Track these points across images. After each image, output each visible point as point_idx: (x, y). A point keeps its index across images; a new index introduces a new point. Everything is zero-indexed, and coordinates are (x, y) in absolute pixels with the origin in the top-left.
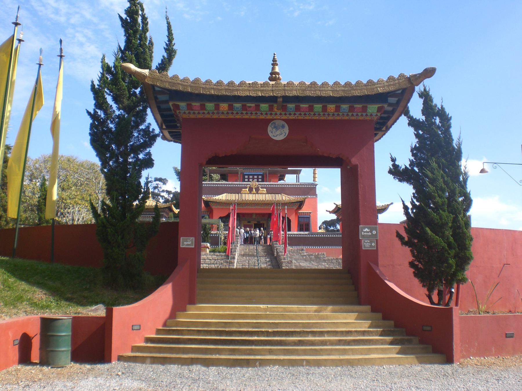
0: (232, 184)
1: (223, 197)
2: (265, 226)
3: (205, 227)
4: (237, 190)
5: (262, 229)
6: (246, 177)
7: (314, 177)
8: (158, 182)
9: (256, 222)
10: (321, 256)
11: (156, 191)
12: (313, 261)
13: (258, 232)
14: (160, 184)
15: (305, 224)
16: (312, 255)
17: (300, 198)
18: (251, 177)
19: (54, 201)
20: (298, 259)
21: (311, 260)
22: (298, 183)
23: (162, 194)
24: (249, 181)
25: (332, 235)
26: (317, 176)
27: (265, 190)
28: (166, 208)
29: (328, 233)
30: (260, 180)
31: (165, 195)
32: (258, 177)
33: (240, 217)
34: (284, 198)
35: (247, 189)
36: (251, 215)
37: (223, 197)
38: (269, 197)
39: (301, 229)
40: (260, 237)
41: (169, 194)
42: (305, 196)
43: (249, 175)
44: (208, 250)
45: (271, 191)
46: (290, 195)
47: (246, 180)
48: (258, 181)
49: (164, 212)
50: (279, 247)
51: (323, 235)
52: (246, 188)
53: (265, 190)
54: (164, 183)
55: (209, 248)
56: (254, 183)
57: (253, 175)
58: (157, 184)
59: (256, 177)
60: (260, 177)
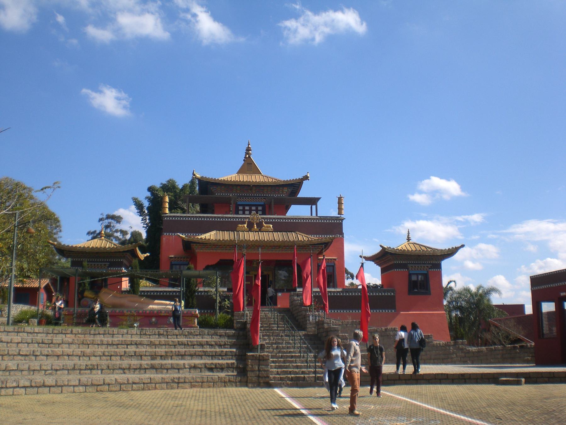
0: (223, 217)
1: (211, 236)
4: (231, 227)
6: (241, 208)
7: (340, 209)
8: (110, 220)
14: (113, 223)
19: (529, 316)
23: (116, 234)
24: (244, 214)
27: (271, 226)
28: (127, 251)
32: (257, 208)
34: (300, 238)
35: (246, 225)
37: (211, 236)
38: (278, 236)
43: (244, 206)
45: (279, 227)
47: (241, 212)
52: (244, 223)
53: (271, 226)
58: (110, 223)
60: (260, 208)
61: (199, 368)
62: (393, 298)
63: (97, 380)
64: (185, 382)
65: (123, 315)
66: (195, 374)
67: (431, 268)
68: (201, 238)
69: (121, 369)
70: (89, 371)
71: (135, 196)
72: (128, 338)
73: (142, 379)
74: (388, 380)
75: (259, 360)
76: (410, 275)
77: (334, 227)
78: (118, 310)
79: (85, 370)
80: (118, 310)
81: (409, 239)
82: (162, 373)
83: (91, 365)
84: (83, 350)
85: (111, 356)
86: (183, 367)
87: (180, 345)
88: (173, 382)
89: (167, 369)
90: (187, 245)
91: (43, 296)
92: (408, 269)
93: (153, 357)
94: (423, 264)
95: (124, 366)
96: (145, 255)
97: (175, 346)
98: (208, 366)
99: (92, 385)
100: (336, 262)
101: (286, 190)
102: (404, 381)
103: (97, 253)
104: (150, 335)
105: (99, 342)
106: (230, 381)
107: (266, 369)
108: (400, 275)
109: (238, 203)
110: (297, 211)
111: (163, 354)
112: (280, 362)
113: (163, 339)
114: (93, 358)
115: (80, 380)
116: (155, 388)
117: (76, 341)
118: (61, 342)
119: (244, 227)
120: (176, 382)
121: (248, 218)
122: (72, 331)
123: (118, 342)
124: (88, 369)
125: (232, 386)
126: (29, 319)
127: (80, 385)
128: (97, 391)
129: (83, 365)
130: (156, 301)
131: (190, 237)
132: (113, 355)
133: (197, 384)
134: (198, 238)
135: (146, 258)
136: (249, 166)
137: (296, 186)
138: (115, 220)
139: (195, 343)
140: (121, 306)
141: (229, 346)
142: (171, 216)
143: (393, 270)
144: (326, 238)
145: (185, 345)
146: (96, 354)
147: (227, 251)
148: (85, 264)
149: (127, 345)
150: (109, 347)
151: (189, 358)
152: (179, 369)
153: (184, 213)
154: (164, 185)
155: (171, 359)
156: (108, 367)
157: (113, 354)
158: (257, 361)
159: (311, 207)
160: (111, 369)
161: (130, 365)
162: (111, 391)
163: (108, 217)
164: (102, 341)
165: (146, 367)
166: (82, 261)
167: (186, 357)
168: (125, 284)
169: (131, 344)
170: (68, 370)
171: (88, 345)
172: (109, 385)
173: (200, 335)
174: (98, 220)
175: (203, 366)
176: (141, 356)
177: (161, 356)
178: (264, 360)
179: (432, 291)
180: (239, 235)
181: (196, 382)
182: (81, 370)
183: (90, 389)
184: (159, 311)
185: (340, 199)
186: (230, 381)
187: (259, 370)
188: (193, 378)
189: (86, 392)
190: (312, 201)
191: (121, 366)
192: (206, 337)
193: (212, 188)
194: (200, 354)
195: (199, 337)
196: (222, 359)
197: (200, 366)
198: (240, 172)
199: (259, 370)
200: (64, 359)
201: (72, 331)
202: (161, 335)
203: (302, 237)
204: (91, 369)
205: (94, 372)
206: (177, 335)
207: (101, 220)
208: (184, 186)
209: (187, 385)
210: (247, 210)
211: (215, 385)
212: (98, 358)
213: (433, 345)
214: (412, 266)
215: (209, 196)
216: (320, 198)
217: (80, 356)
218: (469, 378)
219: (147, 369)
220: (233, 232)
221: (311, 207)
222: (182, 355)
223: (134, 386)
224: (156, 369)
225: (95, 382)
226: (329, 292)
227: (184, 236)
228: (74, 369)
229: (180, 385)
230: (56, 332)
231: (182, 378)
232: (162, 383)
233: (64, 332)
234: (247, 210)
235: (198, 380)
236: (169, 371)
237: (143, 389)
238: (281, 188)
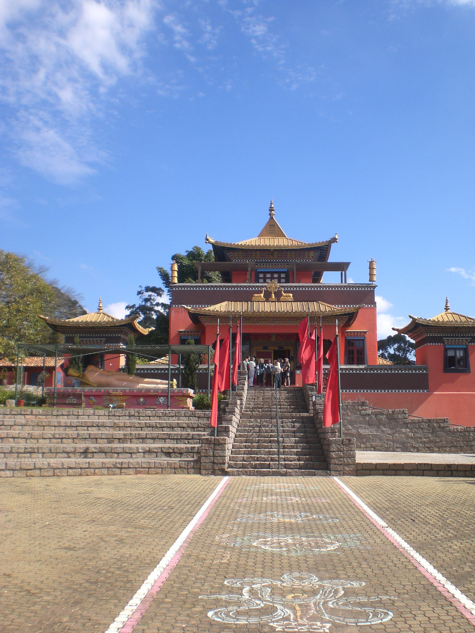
0: (237, 286)
1: (221, 307)
2: (292, 354)
3: (189, 359)
4: (246, 297)
5: (287, 360)
6: (261, 276)
7: (371, 275)
8: (150, 293)
9: (276, 348)
10: (400, 416)
11: (148, 304)
12: (384, 425)
13: (279, 366)
15: (356, 352)
16: (382, 414)
17: (349, 308)
18: (268, 276)
20: (356, 422)
21: (379, 424)
22: (344, 284)
23: (156, 308)
24: (265, 282)
25: (405, 370)
26: (375, 272)
27: (291, 295)
29: (397, 366)
30: (283, 280)
31: (159, 308)
32: (265, 276)
33: (246, 338)
34: (322, 308)
35: (262, 295)
36: (268, 336)
37: (221, 307)
38: (297, 307)
39: (350, 361)
40: (284, 375)
41: (165, 309)
42: (356, 304)
43: (265, 273)
44: (190, 402)
46: (332, 304)
47: (261, 280)
48: (279, 282)
49: (121, 332)
50: (320, 400)
51: (391, 369)
52: (261, 292)
53: (291, 295)
54: (160, 295)
55: (191, 397)
56: (274, 285)
57: (272, 273)
58: (150, 296)
59: (276, 276)
60: (283, 275)
61: (155, 452)
62: (426, 375)
63: (26, 464)
64: (129, 468)
65: (109, 395)
66: (152, 460)
67: (471, 342)
68: (209, 310)
69: (65, 452)
70: (29, 455)
71: (160, 266)
72: (95, 420)
73: (79, 464)
74: (363, 469)
75: (215, 444)
76: (446, 350)
77: (363, 296)
78: (103, 389)
79: (24, 453)
80: (103, 389)
81: (447, 309)
82: (112, 457)
83: (31, 448)
84: (30, 432)
85: (62, 438)
86: (136, 451)
87: (148, 427)
88: (116, 467)
89: (118, 453)
90: (195, 317)
91: (59, 375)
92: (443, 343)
93: (110, 440)
94: (462, 337)
95: (68, 450)
96: (150, 330)
97: (141, 428)
98: (165, 451)
99: (21, 469)
100: (366, 335)
101: (312, 254)
102: (381, 472)
103: (92, 328)
104: (119, 416)
105: (56, 424)
106: (180, 467)
107: (222, 454)
108: (434, 351)
109: (258, 270)
110: (330, 279)
111: (122, 437)
112: (253, 447)
113: (135, 421)
114: (41, 441)
115: (6, 464)
116: (95, 474)
117: (30, 423)
118: (13, 423)
119: (260, 297)
120: (118, 468)
121: (265, 286)
122: (32, 412)
123: (77, 424)
124: (28, 453)
125: (183, 473)
126: (6, 399)
127: (6, 469)
128: (27, 476)
129: (22, 448)
130: (146, 380)
131: (196, 309)
132: (65, 438)
133: (142, 470)
134: (205, 310)
135: (150, 333)
136: (272, 228)
137: (322, 250)
138: (155, 293)
139: (165, 425)
140: (108, 385)
141: (202, 429)
142: (180, 286)
143: (426, 344)
144: (346, 309)
145: (153, 427)
146: (45, 437)
147: (270, 324)
148: (77, 339)
149: (88, 427)
150: (67, 429)
151: (151, 441)
152: (131, 453)
153: (210, 282)
154: (191, 252)
155: (131, 443)
156: (51, 450)
157: (64, 436)
158: (212, 446)
159: (342, 273)
160: (54, 453)
161: (76, 448)
162: (43, 476)
163: (148, 289)
164: (59, 422)
165: (94, 450)
166: (73, 337)
167: (148, 441)
168: (122, 361)
169: (93, 426)
170: (5, 453)
171: (44, 426)
172: (40, 469)
173: (176, 416)
174: (137, 293)
175: (159, 450)
176: (96, 439)
177: (119, 439)
178: (219, 444)
179: (471, 368)
180: (252, 306)
181: (142, 468)
182: (19, 453)
183: (17, 474)
184: (148, 390)
185: (371, 263)
186: (180, 467)
187: (214, 456)
188: (138, 463)
189: (13, 476)
190: (341, 267)
191: (65, 450)
192: (182, 418)
193: (229, 255)
194: (164, 437)
195: (174, 418)
196: (188, 443)
197: (156, 450)
198: (261, 235)
199: (214, 456)
200: (9, 442)
201: (32, 412)
202: (132, 416)
203: (324, 308)
204: (30, 453)
205: (34, 455)
206: (150, 416)
207: (139, 293)
208: (208, 253)
209: (131, 471)
210: (283, 278)
211: (164, 472)
212: (48, 441)
213: (450, 431)
214: (448, 340)
215: (228, 263)
216: (349, 263)
217: (27, 439)
218: (457, 470)
219: (95, 452)
220: (246, 303)
221: (342, 273)
222: (143, 439)
223: (70, 471)
224: (105, 453)
225: (24, 467)
226: (341, 369)
227: (190, 308)
228: (11, 452)
229: (123, 470)
230: (14, 413)
231: (125, 463)
232: (102, 468)
233: (23, 413)
234: (283, 278)
235: (144, 465)
236: (121, 455)
237: (80, 475)
238: (307, 253)
